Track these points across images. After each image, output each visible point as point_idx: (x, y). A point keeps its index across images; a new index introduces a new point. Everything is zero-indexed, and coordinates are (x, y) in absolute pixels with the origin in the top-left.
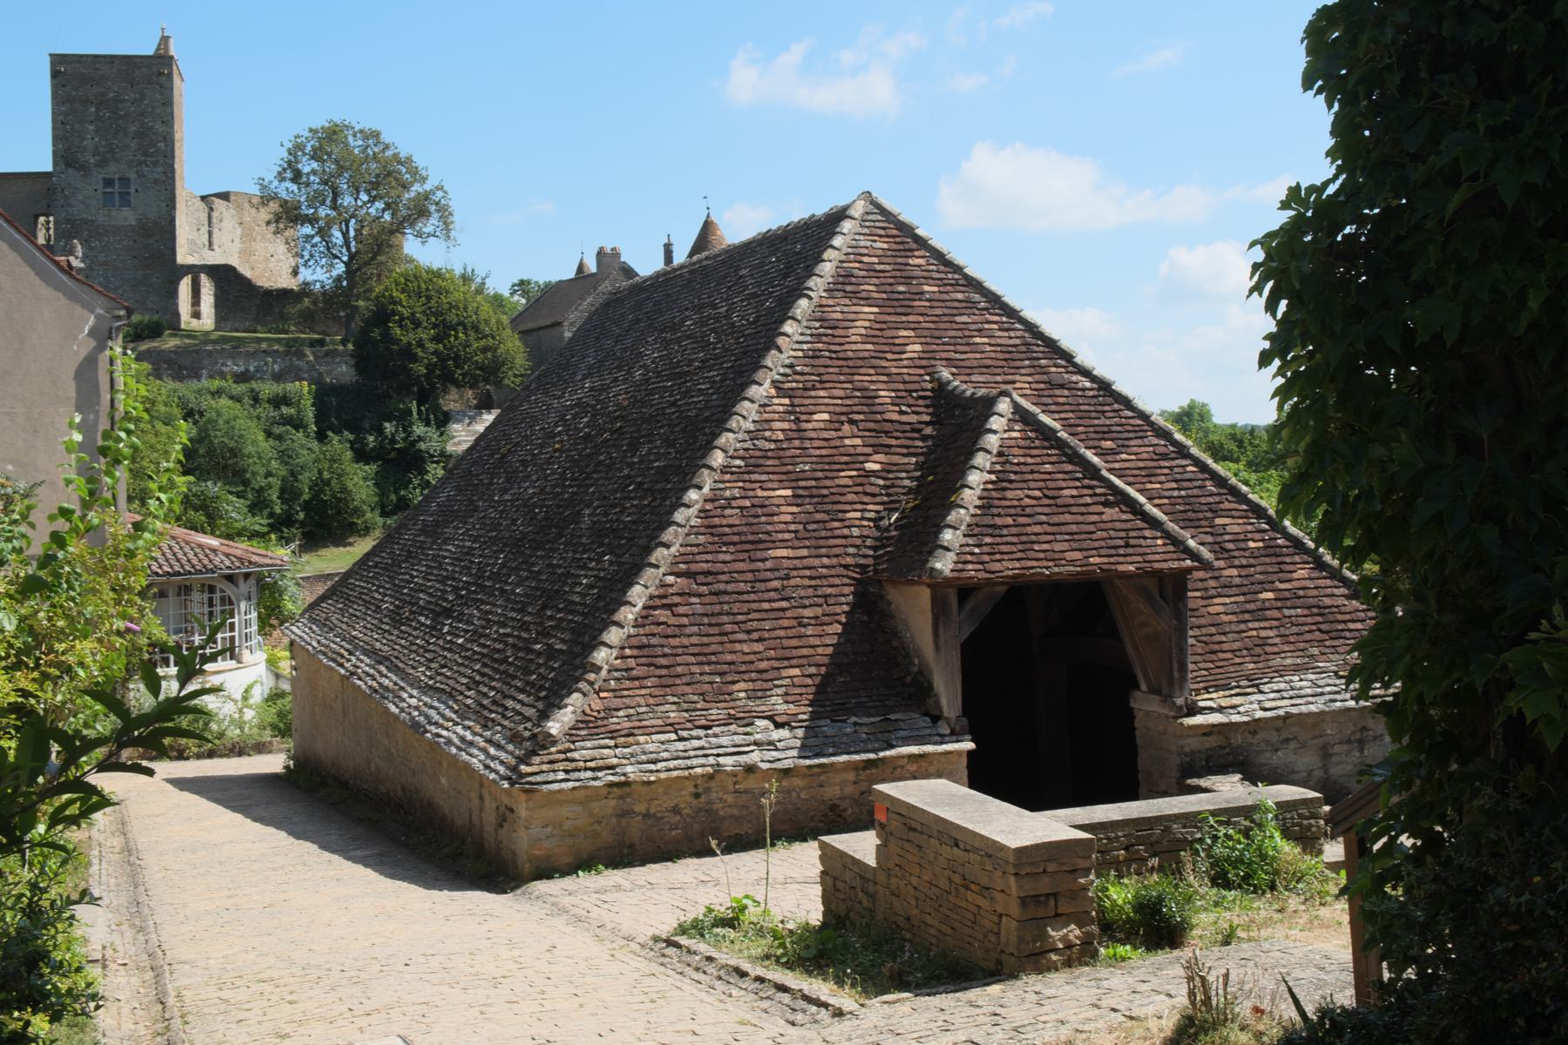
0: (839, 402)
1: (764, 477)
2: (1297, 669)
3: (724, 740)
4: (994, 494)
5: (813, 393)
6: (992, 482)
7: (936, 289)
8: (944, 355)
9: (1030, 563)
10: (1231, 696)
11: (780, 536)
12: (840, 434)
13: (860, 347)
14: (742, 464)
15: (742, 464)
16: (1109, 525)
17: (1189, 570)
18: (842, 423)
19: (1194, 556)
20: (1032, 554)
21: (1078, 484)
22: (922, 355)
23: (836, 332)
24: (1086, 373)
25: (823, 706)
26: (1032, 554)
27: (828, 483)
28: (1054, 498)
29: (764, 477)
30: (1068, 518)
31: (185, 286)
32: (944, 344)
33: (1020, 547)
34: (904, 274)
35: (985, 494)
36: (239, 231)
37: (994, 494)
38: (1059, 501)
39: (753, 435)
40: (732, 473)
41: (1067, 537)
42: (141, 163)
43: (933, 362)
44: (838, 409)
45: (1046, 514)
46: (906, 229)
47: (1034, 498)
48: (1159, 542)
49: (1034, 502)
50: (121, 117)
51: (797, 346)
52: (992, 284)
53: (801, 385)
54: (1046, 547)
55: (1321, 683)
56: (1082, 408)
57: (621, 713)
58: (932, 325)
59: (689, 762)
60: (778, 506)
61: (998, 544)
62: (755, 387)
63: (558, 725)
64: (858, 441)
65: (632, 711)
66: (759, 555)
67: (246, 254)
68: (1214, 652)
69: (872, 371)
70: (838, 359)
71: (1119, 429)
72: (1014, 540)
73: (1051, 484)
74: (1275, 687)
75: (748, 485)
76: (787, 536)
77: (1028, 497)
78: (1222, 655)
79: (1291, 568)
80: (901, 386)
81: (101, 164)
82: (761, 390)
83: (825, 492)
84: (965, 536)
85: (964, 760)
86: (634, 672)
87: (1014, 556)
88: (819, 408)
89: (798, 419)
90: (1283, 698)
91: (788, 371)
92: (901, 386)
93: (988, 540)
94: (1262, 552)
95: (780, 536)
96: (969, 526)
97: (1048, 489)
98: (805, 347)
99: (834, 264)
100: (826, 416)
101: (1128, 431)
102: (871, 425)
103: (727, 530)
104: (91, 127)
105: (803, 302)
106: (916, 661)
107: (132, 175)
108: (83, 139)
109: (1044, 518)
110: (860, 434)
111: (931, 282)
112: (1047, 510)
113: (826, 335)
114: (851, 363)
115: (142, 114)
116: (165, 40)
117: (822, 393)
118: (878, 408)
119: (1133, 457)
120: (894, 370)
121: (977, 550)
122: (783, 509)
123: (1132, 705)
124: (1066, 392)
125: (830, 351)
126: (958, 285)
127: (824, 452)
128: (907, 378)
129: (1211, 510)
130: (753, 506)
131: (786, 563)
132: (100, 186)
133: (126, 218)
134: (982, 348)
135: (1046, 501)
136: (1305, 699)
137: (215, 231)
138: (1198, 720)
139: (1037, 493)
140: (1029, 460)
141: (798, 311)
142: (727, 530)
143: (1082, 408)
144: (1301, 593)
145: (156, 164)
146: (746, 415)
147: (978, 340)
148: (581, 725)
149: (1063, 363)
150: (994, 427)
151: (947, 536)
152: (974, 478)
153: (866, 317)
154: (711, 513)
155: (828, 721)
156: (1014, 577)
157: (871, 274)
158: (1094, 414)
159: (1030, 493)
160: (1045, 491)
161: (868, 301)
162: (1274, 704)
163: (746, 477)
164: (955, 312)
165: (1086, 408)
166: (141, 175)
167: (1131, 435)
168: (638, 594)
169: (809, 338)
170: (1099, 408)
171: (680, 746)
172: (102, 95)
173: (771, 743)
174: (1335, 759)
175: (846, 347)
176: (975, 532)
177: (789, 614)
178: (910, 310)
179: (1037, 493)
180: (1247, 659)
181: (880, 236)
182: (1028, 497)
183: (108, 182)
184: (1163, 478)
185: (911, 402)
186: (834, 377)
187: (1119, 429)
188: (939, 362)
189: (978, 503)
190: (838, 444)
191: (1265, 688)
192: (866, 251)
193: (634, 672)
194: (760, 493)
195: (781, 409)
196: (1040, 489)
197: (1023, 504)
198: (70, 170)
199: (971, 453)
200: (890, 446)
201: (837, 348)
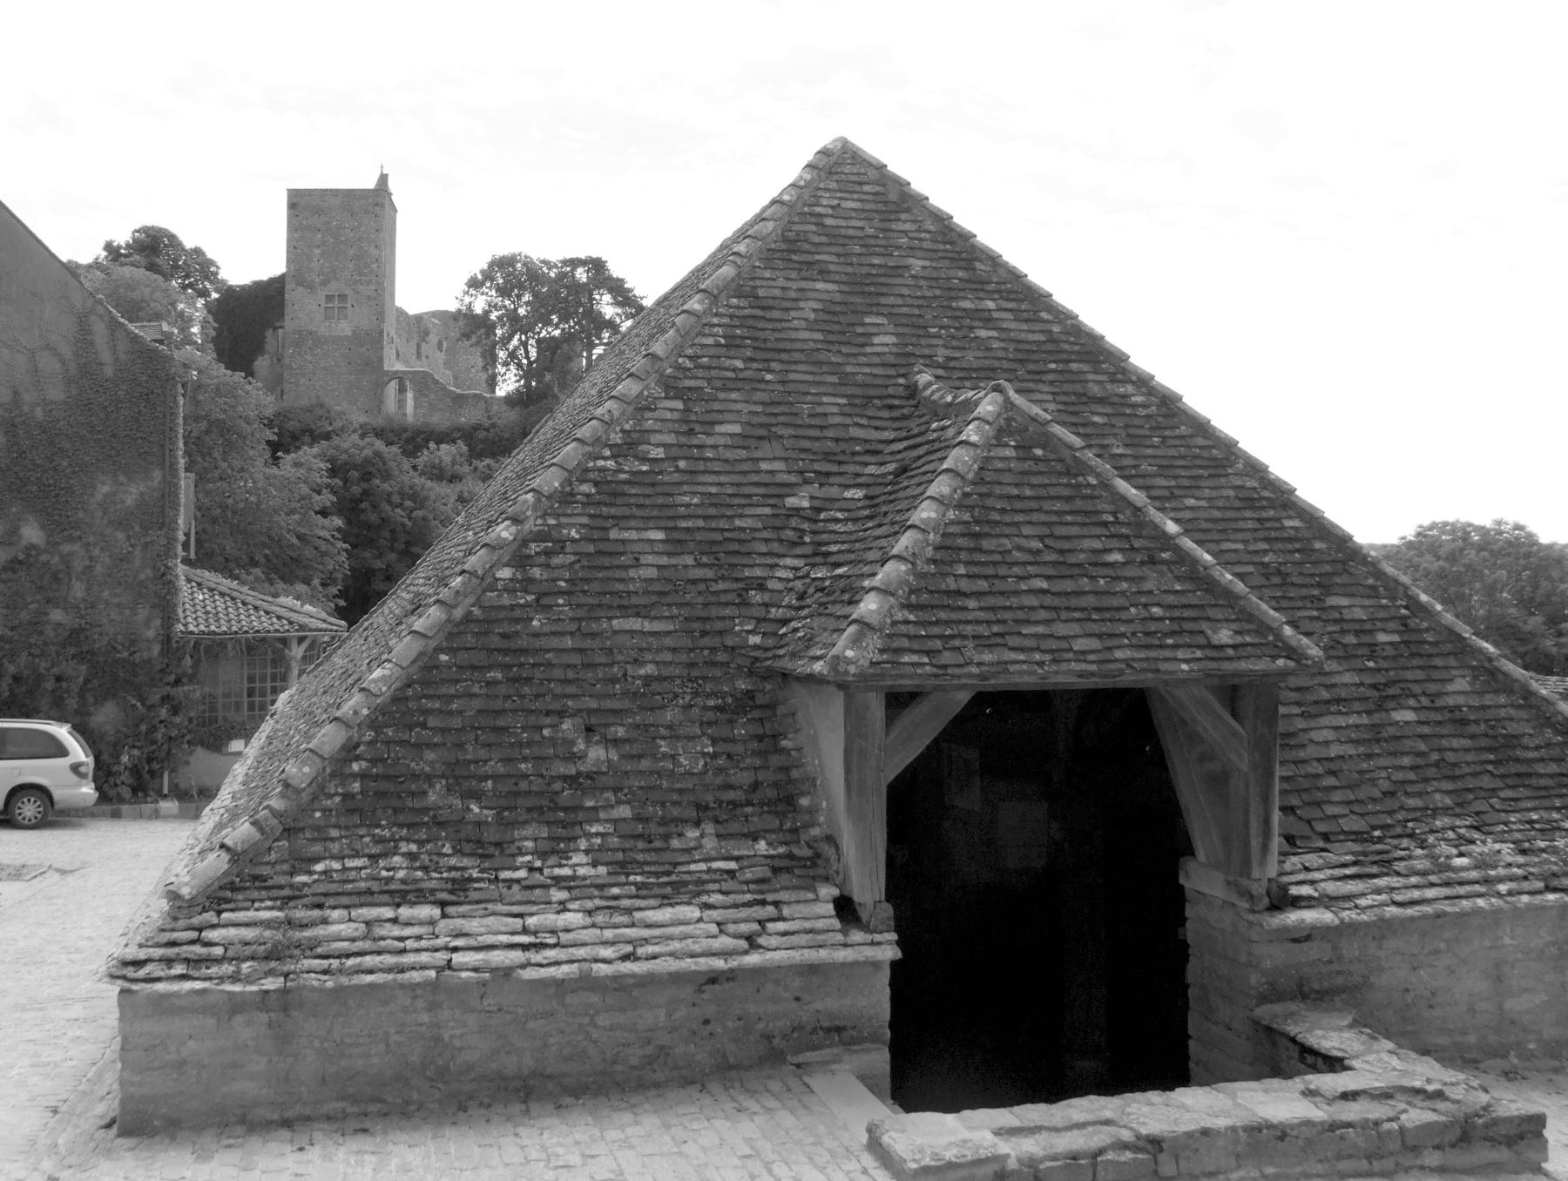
17: (1284, 674)
19: (1292, 653)
28: (1062, 552)
33: (995, 629)
38: (1072, 559)
41: (1077, 615)
47: (1030, 551)
54: (1040, 629)
68: (1318, 804)
77: (1019, 548)
79: (1444, 675)
80: (859, 391)
81: (324, 283)
85: (885, 976)
90: (1432, 885)
97: (1051, 536)
104: (317, 251)
107: (349, 292)
111: (920, 254)
115: (359, 239)
116: (383, 179)
119: (1203, 503)
123: (1182, 881)
129: (1319, 585)
132: (323, 302)
133: (343, 330)
136: (1468, 888)
138: (1293, 917)
145: (369, 282)
153: (816, 295)
161: (824, 274)
166: (356, 292)
172: (328, 223)
178: (884, 290)
182: (1019, 548)
183: (329, 298)
184: (1248, 536)
197: (1008, 559)
198: (300, 289)
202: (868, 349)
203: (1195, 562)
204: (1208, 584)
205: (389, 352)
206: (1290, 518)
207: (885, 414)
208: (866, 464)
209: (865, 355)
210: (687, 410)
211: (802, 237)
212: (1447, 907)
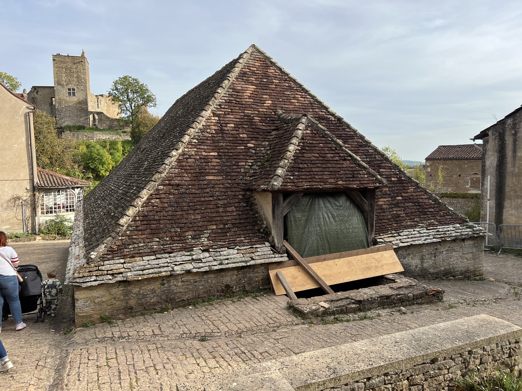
0: (239, 120)
1: (206, 147)
2: (411, 227)
3: (178, 259)
4: (300, 155)
5: (228, 116)
6: (299, 150)
7: (278, 81)
8: (280, 105)
9: (314, 183)
10: (389, 237)
11: (211, 171)
12: (238, 132)
13: (248, 100)
14: (197, 142)
15: (197, 142)
16: (346, 169)
18: (239, 128)
20: (315, 180)
21: (333, 152)
22: (272, 105)
23: (239, 94)
24: (333, 115)
25: (225, 242)
26: (315, 180)
27: (232, 151)
28: (323, 157)
29: (206, 147)
30: (329, 165)
31: (91, 116)
32: (280, 101)
33: (310, 177)
34: (266, 75)
35: (296, 155)
36: (106, 105)
37: (300, 155)
38: (326, 159)
39: (202, 131)
40: (192, 145)
42: (78, 85)
43: (276, 108)
44: (238, 123)
45: (320, 164)
46: (268, 58)
47: (316, 157)
48: (366, 176)
49: (316, 159)
50: (72, 72)
51: (223, 98)
52: (299, 81)
53: (223, 113)
54: (320, 177)
55: (422, 232)
56: (331, 127)
57: (130, 247)
58: (276, 94)
59: (160, 270)
60: (211, 159)
61: (301, 175)
62: (204, 112)
63: (95, 254)
64: (245, 136)
65: (136, 246)
66: (201, 178)
67: (108, 110)
68: (381, 220)
69: (252, 109)
70: (239, 104)
71: (344, 135)
72: (307, 173)
73: (322, 152)
74: (405, 233)
75: (199, 150)
76: (214, 171)
77: (313, 156)
78: (384, 221)
82: (207, 113)
83: (231, 154)
84: (287, 171)
86: (140, 227)
87: (308, 180)
88: (230, 122)
89: (221, 125)
90: (409, 238)
91: (218, 107)
92: (263, 116)
93: (296, 173)
94: (397, 182)
95: (211, 171)
96: (289, 167)
98: (226, 98)
99: (240, 69)
100: (233, 125)
101: (348, 137)
102: (251, 130)
103: (188, 168)
105: (226, 82)
106: (265, 223)
107: (76, 88)
108: (62, 78)
109: (319, 165)
110: (246, 133)
112: (321, 162)
113: (235, 95)
114: (244, 106)
115: (78, 72)
117: (232, 117)
118: (254, 123)
119: (349, 146)
120: (261, 110)
121: (292, 178)
122: (213, 160)
124: (325, 122)
125: (236, 101)
126: (286, 80)
127: (231, 139)
128: (266, 113)
130: (200, 158)
131: (213, 182)
134: (294, 104)
135: (321, 159)
137: (99, 104)
139: (317, 155)
140: (314, 142)
141: (224, 84)
142: (188, 168)
143: (331, 127)
144: (411, 197)
146: (201, 123)
147: (293, 101)
148: (109, 253)
149: (325, 111)
150: (300, 128)
151: (280, 171)
152: (291, 148)
154: (182, 161)
155: (226, 249)
156: (307, 189)
157: (254, 74)
158: (336, 130)
159: (314, 155)
160: (321, 155)
161: (252, 84)
162: (405, 240)
163: (198, 147)
164: (285, 90)
165: (333, 127)
166: (78, 88)
167: (349, 138)
168: (145, 194)
169: (228, 95)
170: (337, 128)
171: (156, 262)
172: (67, 66)
173: (200, 260)
174: (425, 261)
175: (242, 100)
176: (291, 170)
177: (213, 203)
179: (317, 155)
180: (393, 222)
181: (258, 61)
182: (313, 156)
183: (69, 89)
185: (267, 122)
186: (237, 111)
187: (344, 135)
188: (278, 108)
189: (292, 158)
190: (237, 136)
191: (402, 234)
192: (252, 66)
193: (140, 227)
194: (204, 153)
195: (215, 121)
196: (318, 154)
198: (59, 86)
199: (291, 138)
200: (258, 138)
201: (239, 100)
202: (265, 105)
203: (356, 159)
204: (360, 165)
205: (90, 104)
206: (370, 150)
207: (271, 122)
208: (267, 136)
209: (264, 106)
210: (219, 120)
211: (245, 73)
212: (413, 243)
